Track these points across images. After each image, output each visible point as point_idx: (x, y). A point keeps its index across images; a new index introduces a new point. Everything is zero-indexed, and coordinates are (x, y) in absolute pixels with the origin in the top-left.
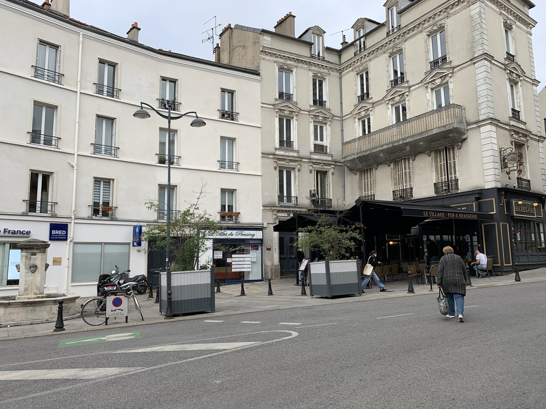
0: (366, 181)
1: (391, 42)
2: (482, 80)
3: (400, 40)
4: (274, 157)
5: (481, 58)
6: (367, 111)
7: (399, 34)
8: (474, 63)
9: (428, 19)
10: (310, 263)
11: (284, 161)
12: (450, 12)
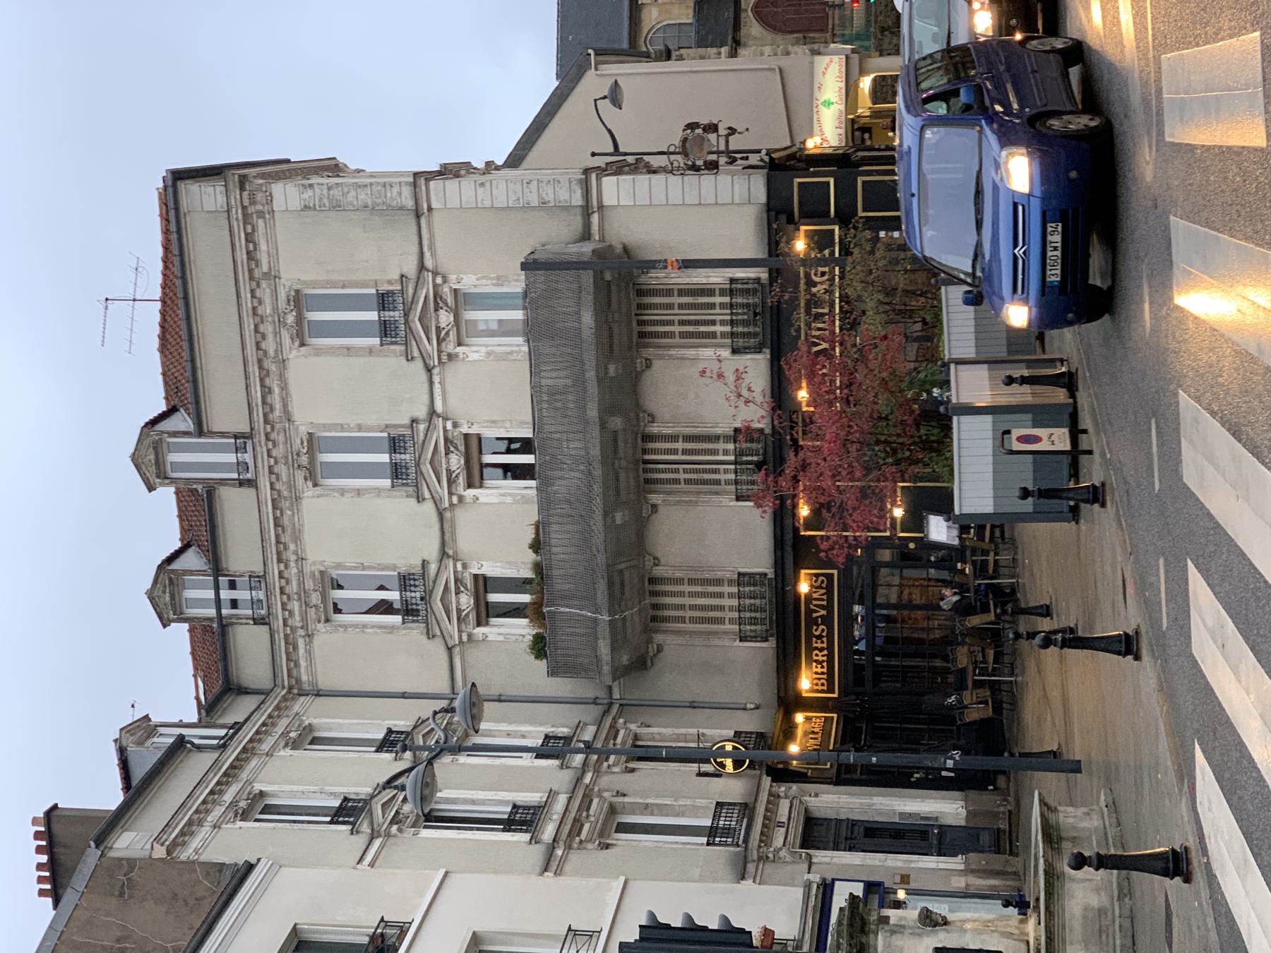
0: (689, 614)
1: (276, 470)
2: (480, 190)
3: (281, 438)
4: (561, 844)
5: (424, 188)
6: (461, 583)
7: (263, 438)
8: (430, 209)
9: (258, 335)
10: (957, 512)
11: (582, 825)
12: (265, 269)
